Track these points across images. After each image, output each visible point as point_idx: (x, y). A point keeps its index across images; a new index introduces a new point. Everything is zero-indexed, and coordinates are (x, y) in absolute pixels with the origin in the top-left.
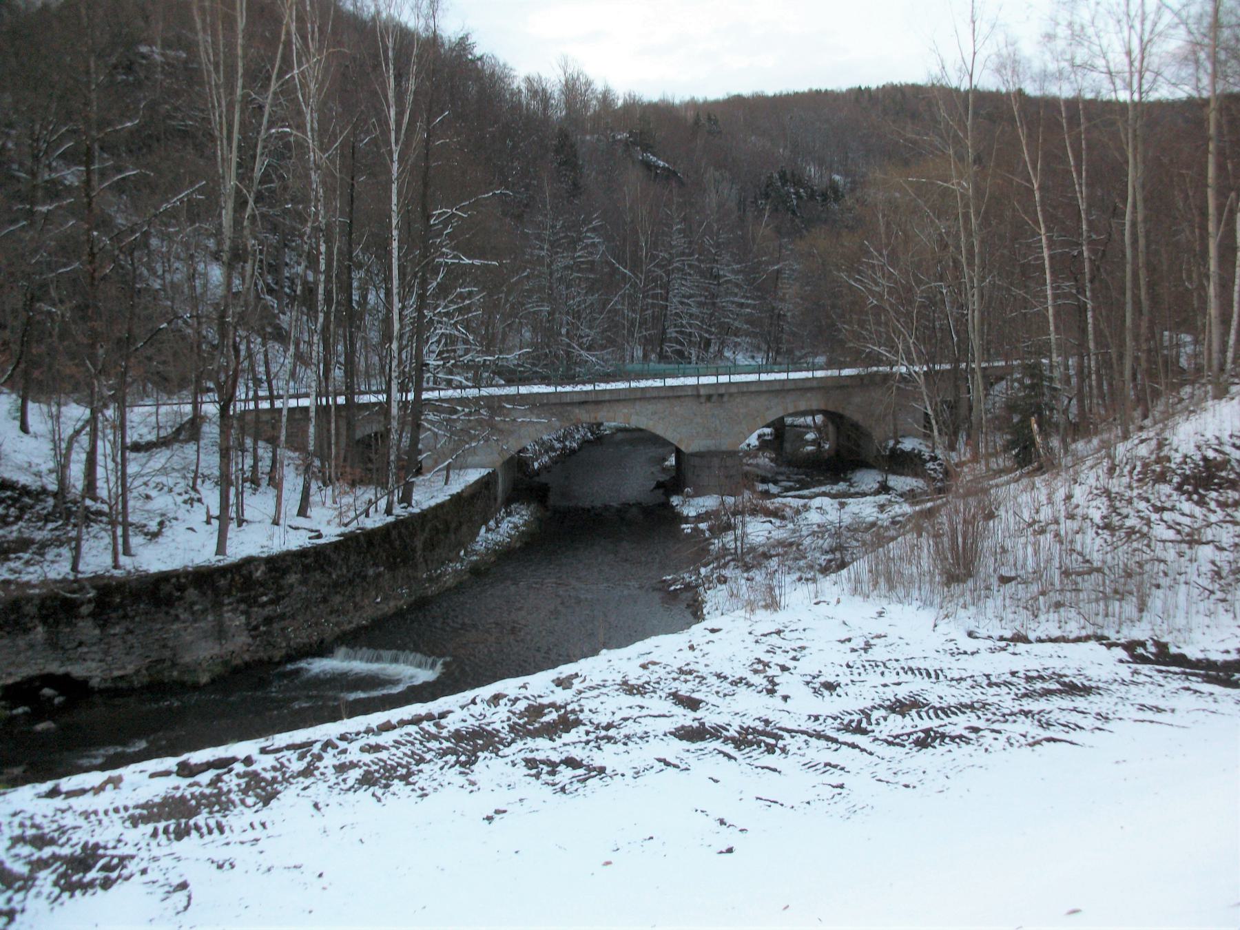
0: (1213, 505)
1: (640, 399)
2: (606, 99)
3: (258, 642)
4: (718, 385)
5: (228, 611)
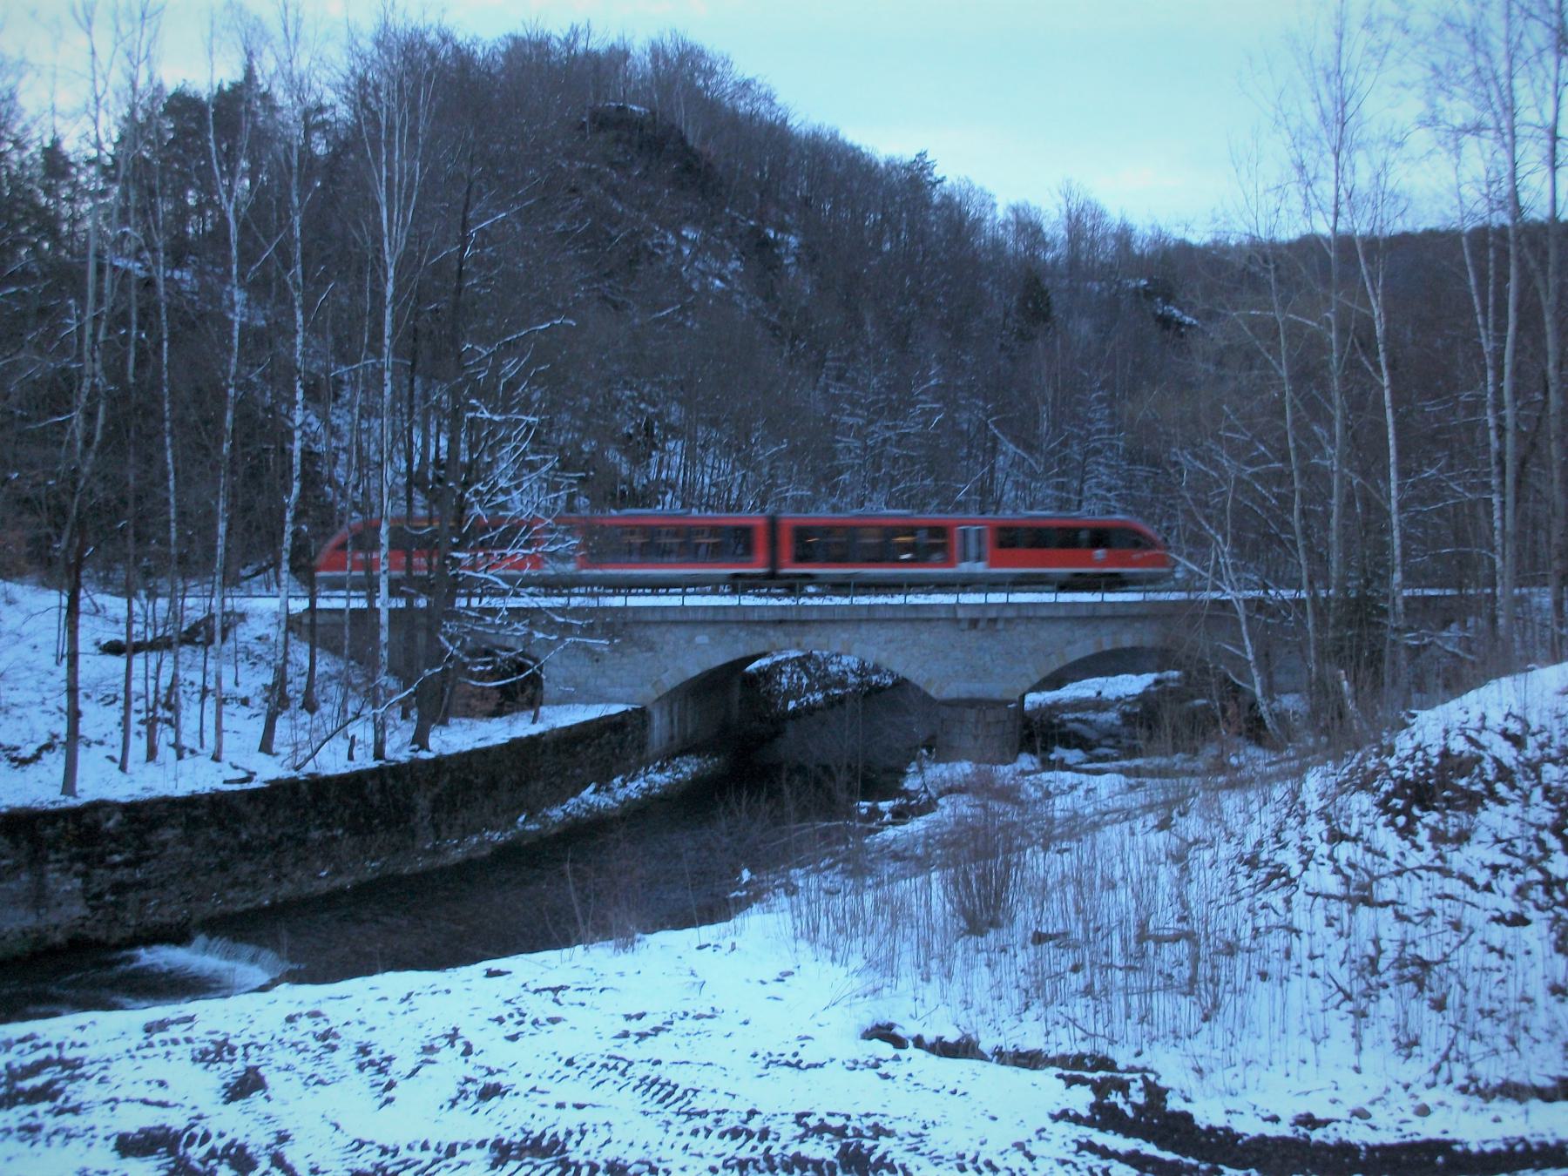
0: (1423, 837)
1: (868, 621)
2: (1124, 237)
3: (99, 916)
4: (987, 605)
5: (54, 871)
